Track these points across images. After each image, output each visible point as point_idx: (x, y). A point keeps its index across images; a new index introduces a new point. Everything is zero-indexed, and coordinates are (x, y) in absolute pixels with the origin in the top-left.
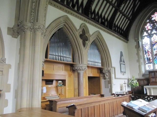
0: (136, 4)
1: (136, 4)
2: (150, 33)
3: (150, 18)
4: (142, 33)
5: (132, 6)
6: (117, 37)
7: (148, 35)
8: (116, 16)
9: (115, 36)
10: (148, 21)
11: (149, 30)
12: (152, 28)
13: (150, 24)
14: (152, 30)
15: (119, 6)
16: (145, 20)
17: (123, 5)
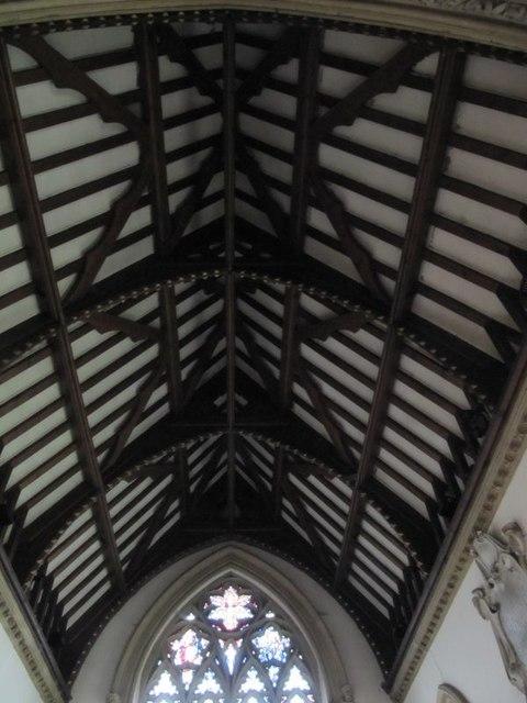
0: (169, 512)
1: (169, 512)
2: (275, 685)
3: (201, 606)
4: (151, 674)
5: (150, 513)
6: (24, 650)
7: (306, 693)
8: (73, 518)
9: (18, 635)
10: (191, 617)
11: (188, 666)
12: (205, 659)
13: (199, 637)
14: (199, 673)
15: (110, 477)
16: (182, 609)
17: (123, 485)
